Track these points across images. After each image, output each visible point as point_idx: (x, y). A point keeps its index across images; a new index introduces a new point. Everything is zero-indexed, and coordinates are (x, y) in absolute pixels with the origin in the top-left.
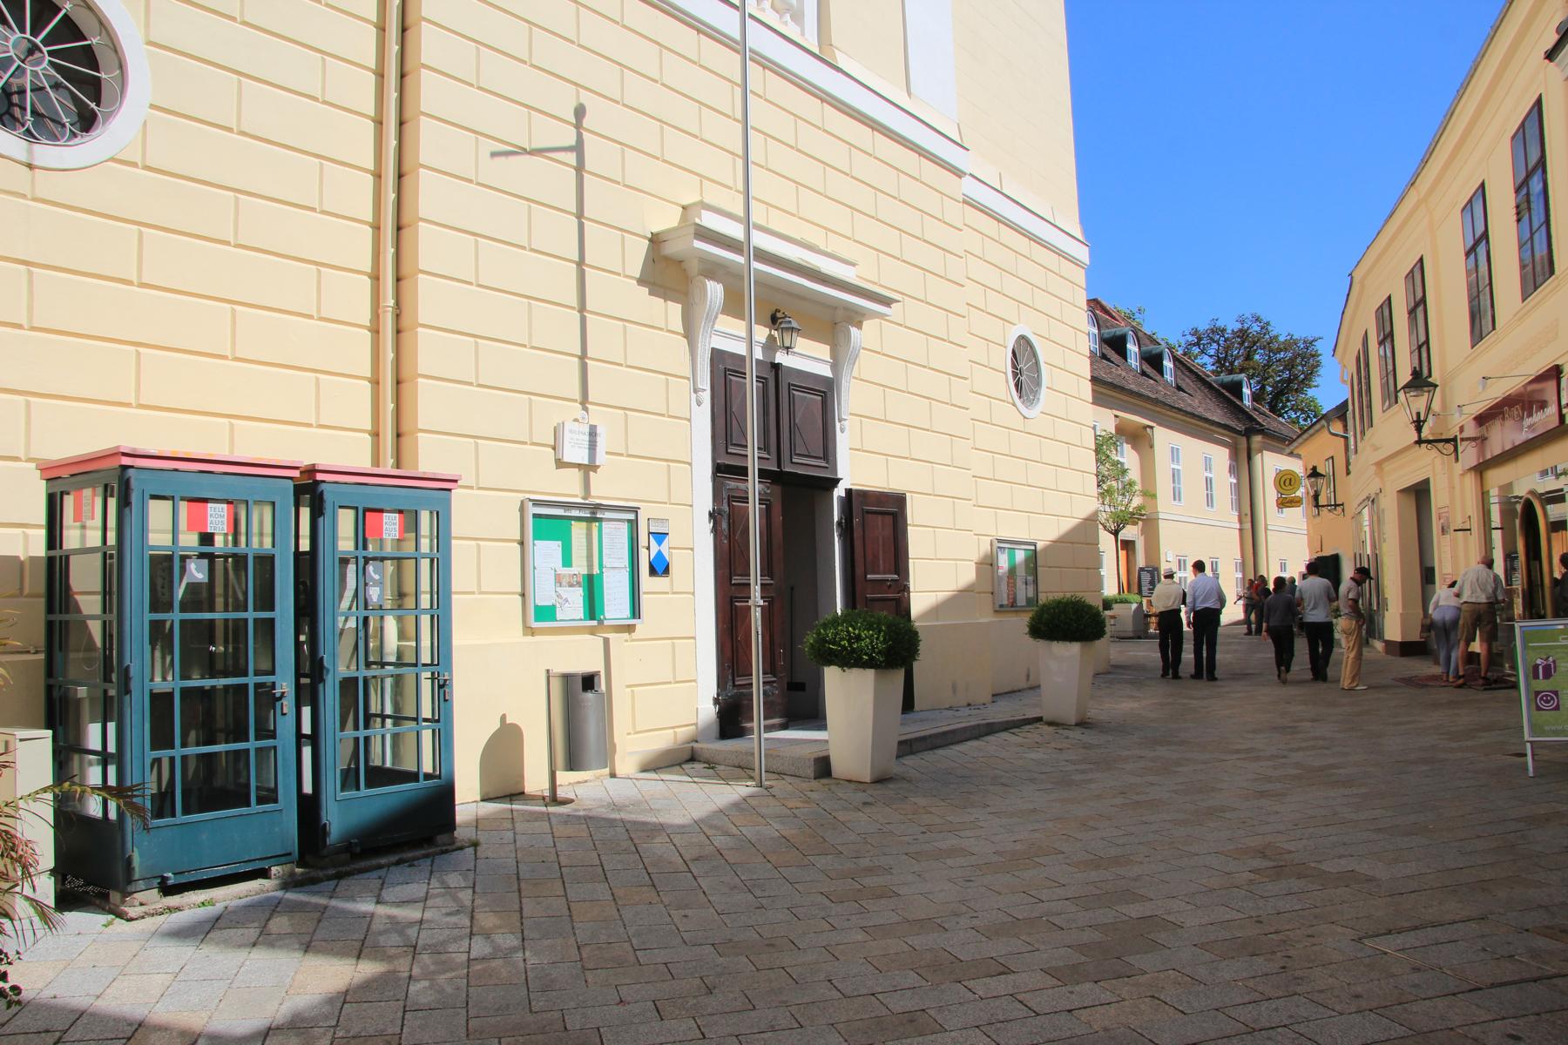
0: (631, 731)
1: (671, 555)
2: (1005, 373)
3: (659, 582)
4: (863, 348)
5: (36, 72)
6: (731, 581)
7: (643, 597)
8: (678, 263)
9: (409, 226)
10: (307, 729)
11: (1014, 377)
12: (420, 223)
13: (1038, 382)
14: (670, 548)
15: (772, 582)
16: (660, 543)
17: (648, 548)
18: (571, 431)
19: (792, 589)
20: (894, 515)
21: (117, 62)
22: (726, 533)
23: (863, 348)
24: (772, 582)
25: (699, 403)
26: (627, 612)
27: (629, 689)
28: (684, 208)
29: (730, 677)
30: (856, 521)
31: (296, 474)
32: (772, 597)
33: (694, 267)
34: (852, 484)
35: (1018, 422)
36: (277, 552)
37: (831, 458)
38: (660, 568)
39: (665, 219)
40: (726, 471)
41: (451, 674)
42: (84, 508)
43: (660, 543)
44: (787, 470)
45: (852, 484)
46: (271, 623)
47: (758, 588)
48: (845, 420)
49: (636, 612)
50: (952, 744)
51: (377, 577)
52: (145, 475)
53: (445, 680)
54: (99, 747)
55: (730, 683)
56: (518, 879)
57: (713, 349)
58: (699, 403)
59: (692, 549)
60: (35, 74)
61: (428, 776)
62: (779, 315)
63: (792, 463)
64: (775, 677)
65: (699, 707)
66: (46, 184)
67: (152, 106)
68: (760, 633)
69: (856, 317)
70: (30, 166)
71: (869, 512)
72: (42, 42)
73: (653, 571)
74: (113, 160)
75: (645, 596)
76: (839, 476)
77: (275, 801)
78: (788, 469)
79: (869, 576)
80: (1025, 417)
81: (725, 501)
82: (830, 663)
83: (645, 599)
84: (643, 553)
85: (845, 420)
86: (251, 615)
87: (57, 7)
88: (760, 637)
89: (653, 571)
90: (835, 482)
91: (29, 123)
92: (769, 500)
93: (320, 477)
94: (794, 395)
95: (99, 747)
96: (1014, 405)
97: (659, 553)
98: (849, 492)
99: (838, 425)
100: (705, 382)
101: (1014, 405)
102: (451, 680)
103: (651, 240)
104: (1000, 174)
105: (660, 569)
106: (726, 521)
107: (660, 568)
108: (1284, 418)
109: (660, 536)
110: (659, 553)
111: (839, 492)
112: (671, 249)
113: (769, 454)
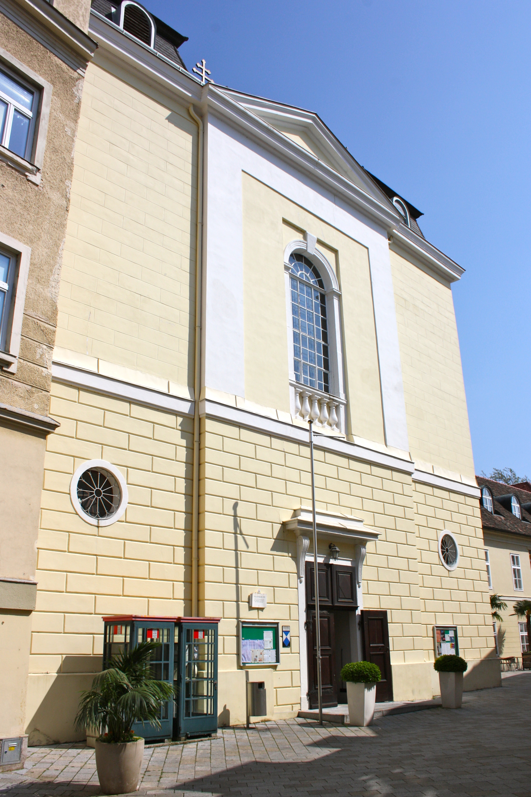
0: (276, 705)
1: (291, 639)
2: (438, 552)
3: (287, 650)
4: (367, 553)
5: (97, 498)
6: (314, 648)
7: (281, 655)
8: (292, 532)
9: (202, 531)
10: (247, 665)
11: (443, 553)
12: (206, 531)
13: (456, 554)
14: (290, 637)
15: (330, 648)
16: (286, 635)
17: (282, 637)
18: (255, 596)
19: (342, 650)
20: (381, 619)
21: (119, 492)
22: (312, 630)
23: (367, 553)
24: (330, 648)
25: (301, 582)
26: (275, 661)
27: (275, 689)
28: (295, 510)
29: (314, 685)
30: (365, 623)
31: (175, 620)
32: (330, 655)
33: (298, 533)
34: (364, 608)
35: (446, 573)
36: (170, 643)
37: (354, 598)
38: (287, 644)
39: (287, 517)
40: (310, 608)
41: (217, 681)
42: (118, 631)
43: (286, 635)
44: (336, 605)
45: (364, 608)
46: (168, 664)
47: (320, 652)
48: (360, 583)
49: (278, 660)
50: (401, 713)
51: (196, 650)
52: (138, 623)
53: (216, 683)
54: (206, 677)
55: (313, 688)
56: (238, 746)
57: (306, 561)
58: (301, 582)
59: (299, 637)
60: (96, 499)
61: (209, 714)
62: (332, 545)
63: (338, 601)
64: (332, 685)
65: (301, 696)
66: (102, 531)
67: (129, 503)
68: (320, 668)
69: (363, 543)
70: (98, 527)
71: (371, 619)
72: (103, 494)
73: (284, 646)
74: (118, 521)
75: (281, 655)
76: (358, 606)
77: (167, 719)
78: (336, 604)
79: (371, 645)
80: (449, 571)
81: (311, 618)
82: (348, 680)
83: (281, 656)
84: (280, 639)
85: (360, 583)
86: (163, 662)
87: (112, 492)
88: (320, 670)
89: (284, 646)
90: (356, 608)
91: (98, 514)
92: (329, 617)
93: (182, 621)
94: (338, 575)
95: (206, 677)
96: (443, 565)
97: (286, 639)
98: (362, 611)
99: (357, 585)
100: (303, 575)
101: (443, 565)
102: (217, 683)
103: (282, 524)
104: (433, 466)
105: (287, 645)
106: (312, 625)
107: (287, 644)
108: (99, 709)
109: (287, 633)
110: (286, 639)
111: (358, 612)
112: (291, 527)
113: (328, 599)
